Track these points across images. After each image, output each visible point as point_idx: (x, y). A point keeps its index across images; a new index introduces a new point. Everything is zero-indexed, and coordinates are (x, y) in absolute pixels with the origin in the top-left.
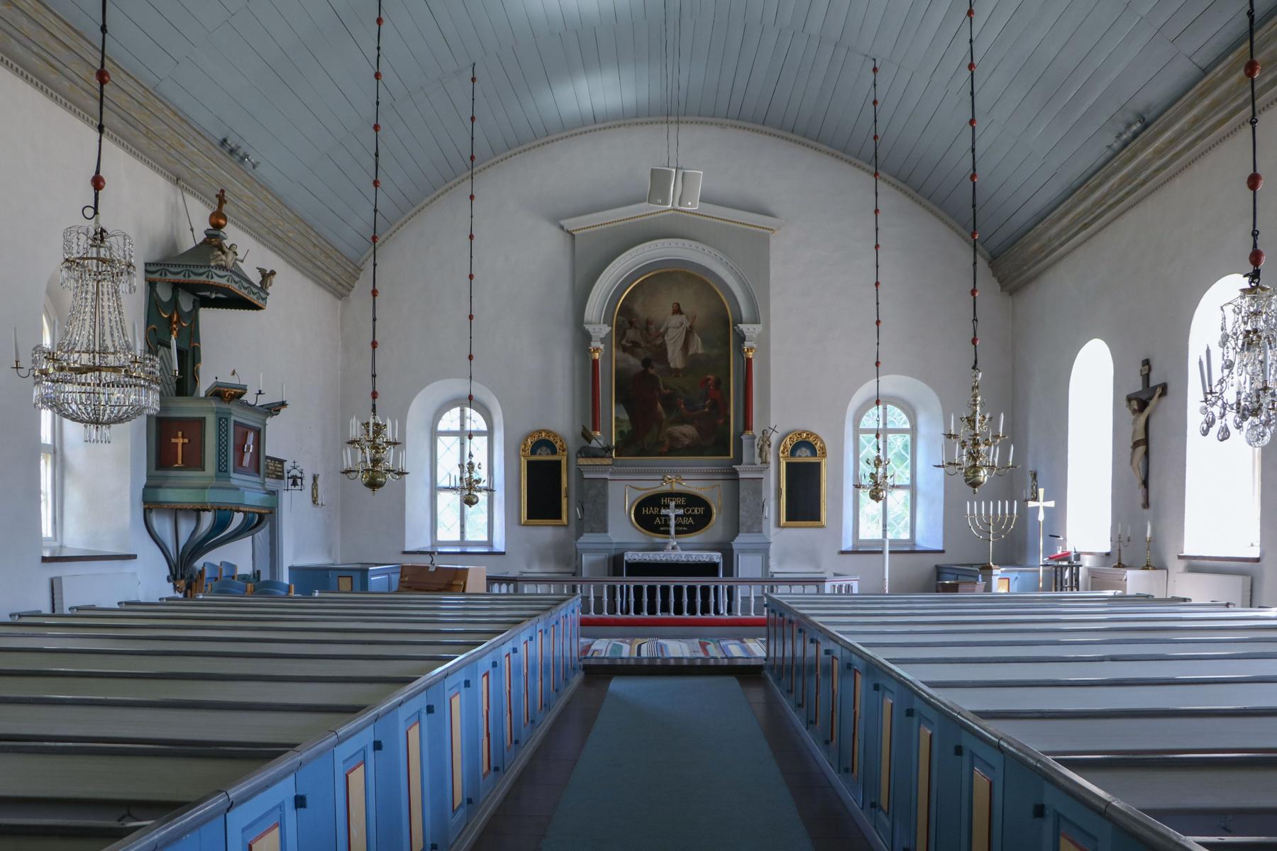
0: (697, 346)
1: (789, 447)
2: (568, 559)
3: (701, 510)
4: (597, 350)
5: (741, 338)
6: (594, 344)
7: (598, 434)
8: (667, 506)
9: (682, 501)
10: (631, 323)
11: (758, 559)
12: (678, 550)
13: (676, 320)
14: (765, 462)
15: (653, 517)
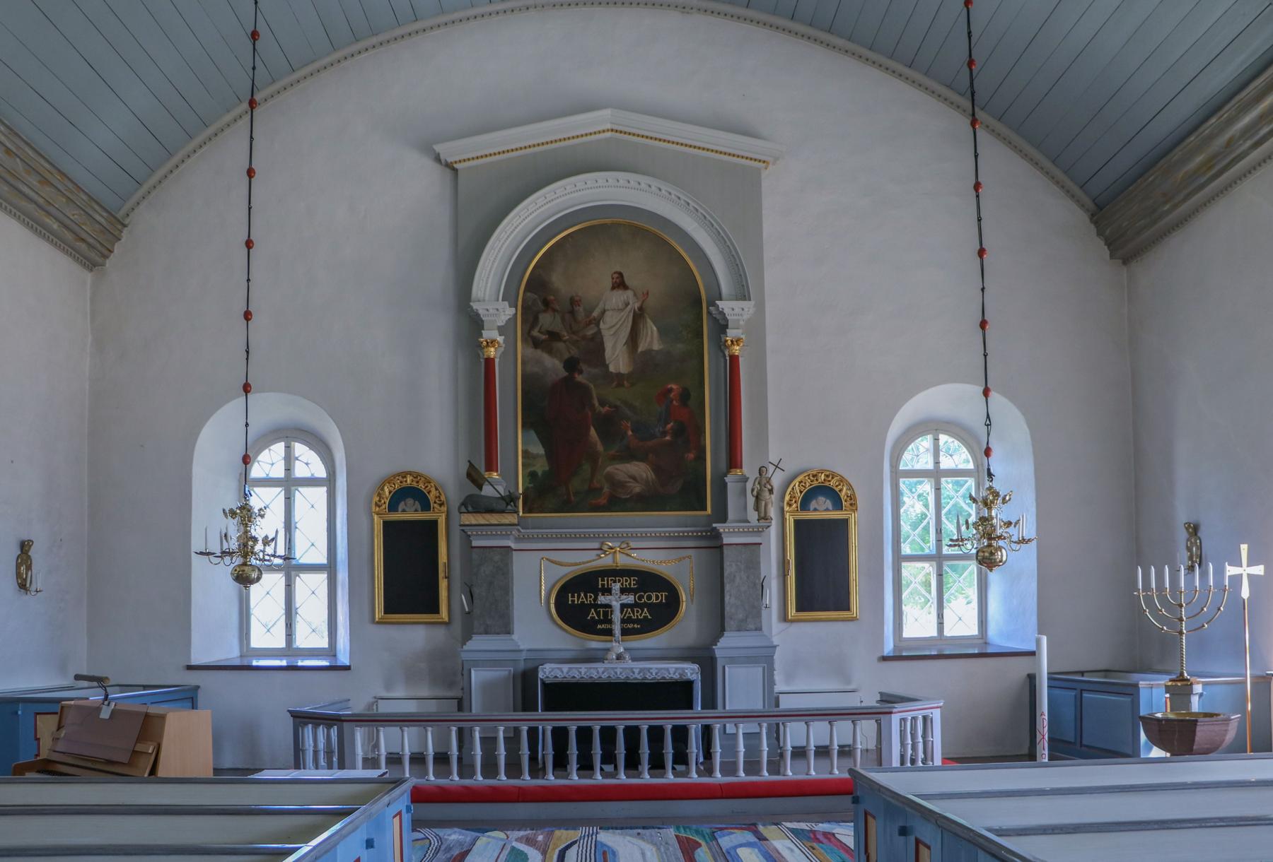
0: (651, 339)
1: (799, 496)
2: (448, 674)
3: (663, 596)
4: (492, 342)
5: (721, 326)
6: (488, 334)
7: (495, 475)
8: (608, 591)
9: (632, 582)
10: (547, 303)
11: (757, 672)
12: (625, 659)
13: (618, 298)
14: (764, 518)
15: (585, 608)
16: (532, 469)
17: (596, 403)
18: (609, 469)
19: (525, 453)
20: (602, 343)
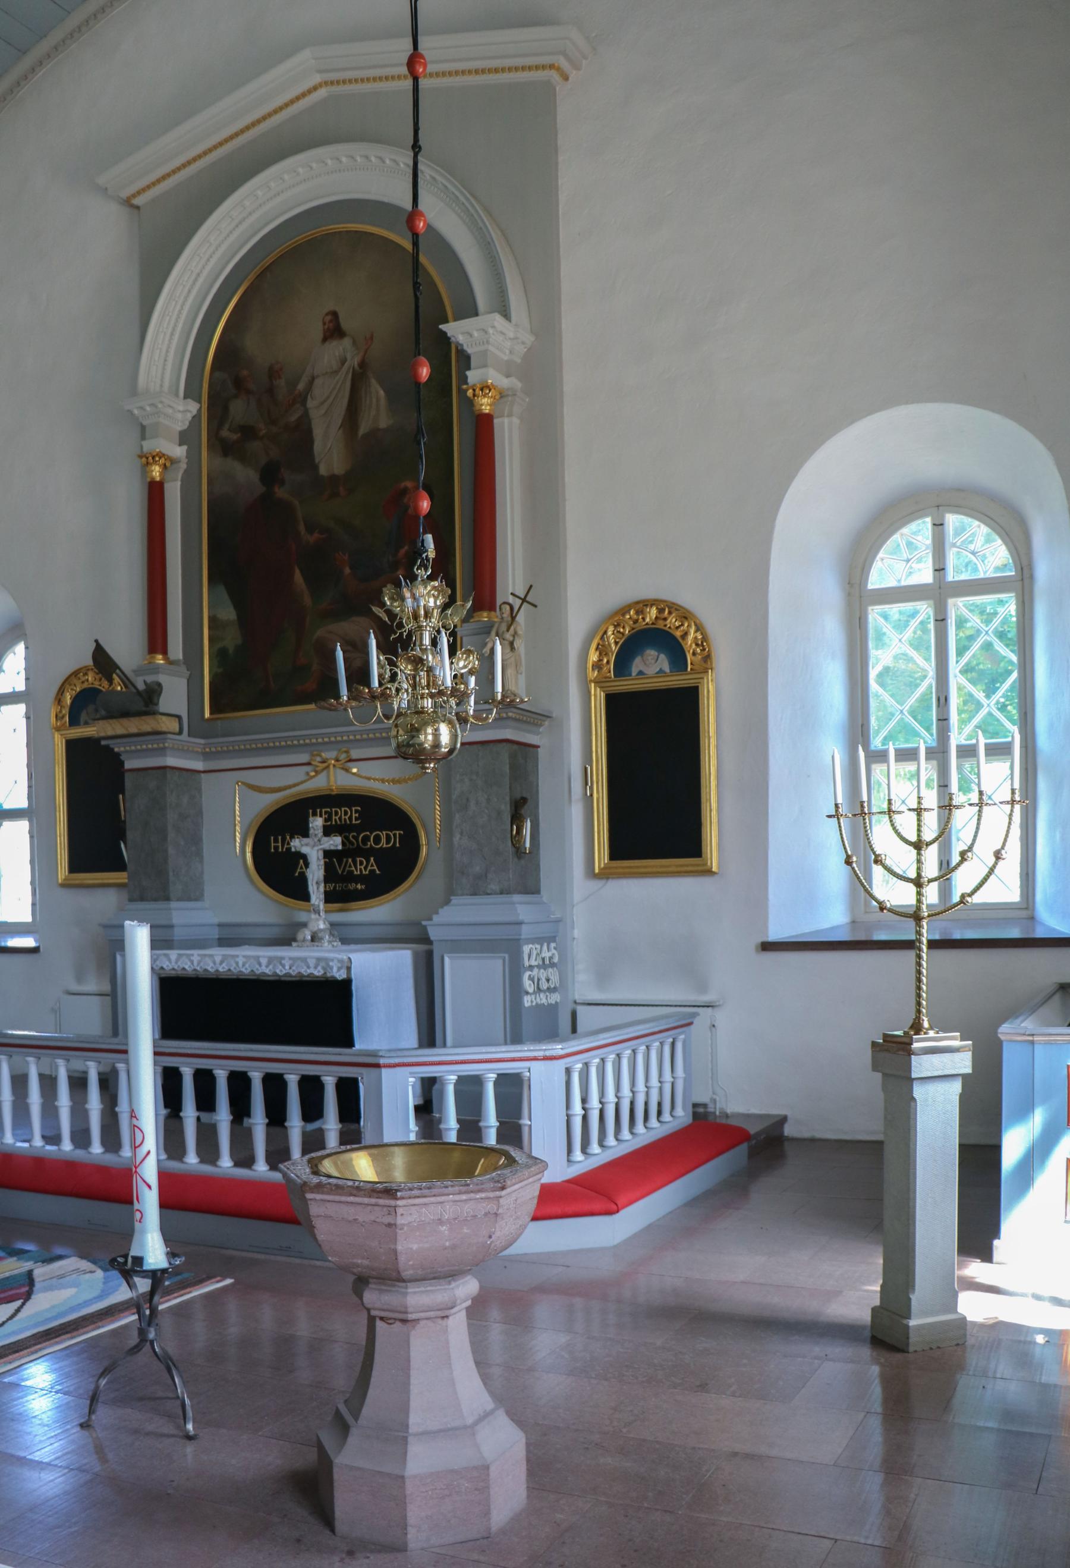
0: (378, 413)
8: (305, 833)
9: (350, 815)
10: (239, 384)
11: (495, 966)
17: (302, 528)
18: (319, 633)
19: (212, 620)
20: (309, 431)
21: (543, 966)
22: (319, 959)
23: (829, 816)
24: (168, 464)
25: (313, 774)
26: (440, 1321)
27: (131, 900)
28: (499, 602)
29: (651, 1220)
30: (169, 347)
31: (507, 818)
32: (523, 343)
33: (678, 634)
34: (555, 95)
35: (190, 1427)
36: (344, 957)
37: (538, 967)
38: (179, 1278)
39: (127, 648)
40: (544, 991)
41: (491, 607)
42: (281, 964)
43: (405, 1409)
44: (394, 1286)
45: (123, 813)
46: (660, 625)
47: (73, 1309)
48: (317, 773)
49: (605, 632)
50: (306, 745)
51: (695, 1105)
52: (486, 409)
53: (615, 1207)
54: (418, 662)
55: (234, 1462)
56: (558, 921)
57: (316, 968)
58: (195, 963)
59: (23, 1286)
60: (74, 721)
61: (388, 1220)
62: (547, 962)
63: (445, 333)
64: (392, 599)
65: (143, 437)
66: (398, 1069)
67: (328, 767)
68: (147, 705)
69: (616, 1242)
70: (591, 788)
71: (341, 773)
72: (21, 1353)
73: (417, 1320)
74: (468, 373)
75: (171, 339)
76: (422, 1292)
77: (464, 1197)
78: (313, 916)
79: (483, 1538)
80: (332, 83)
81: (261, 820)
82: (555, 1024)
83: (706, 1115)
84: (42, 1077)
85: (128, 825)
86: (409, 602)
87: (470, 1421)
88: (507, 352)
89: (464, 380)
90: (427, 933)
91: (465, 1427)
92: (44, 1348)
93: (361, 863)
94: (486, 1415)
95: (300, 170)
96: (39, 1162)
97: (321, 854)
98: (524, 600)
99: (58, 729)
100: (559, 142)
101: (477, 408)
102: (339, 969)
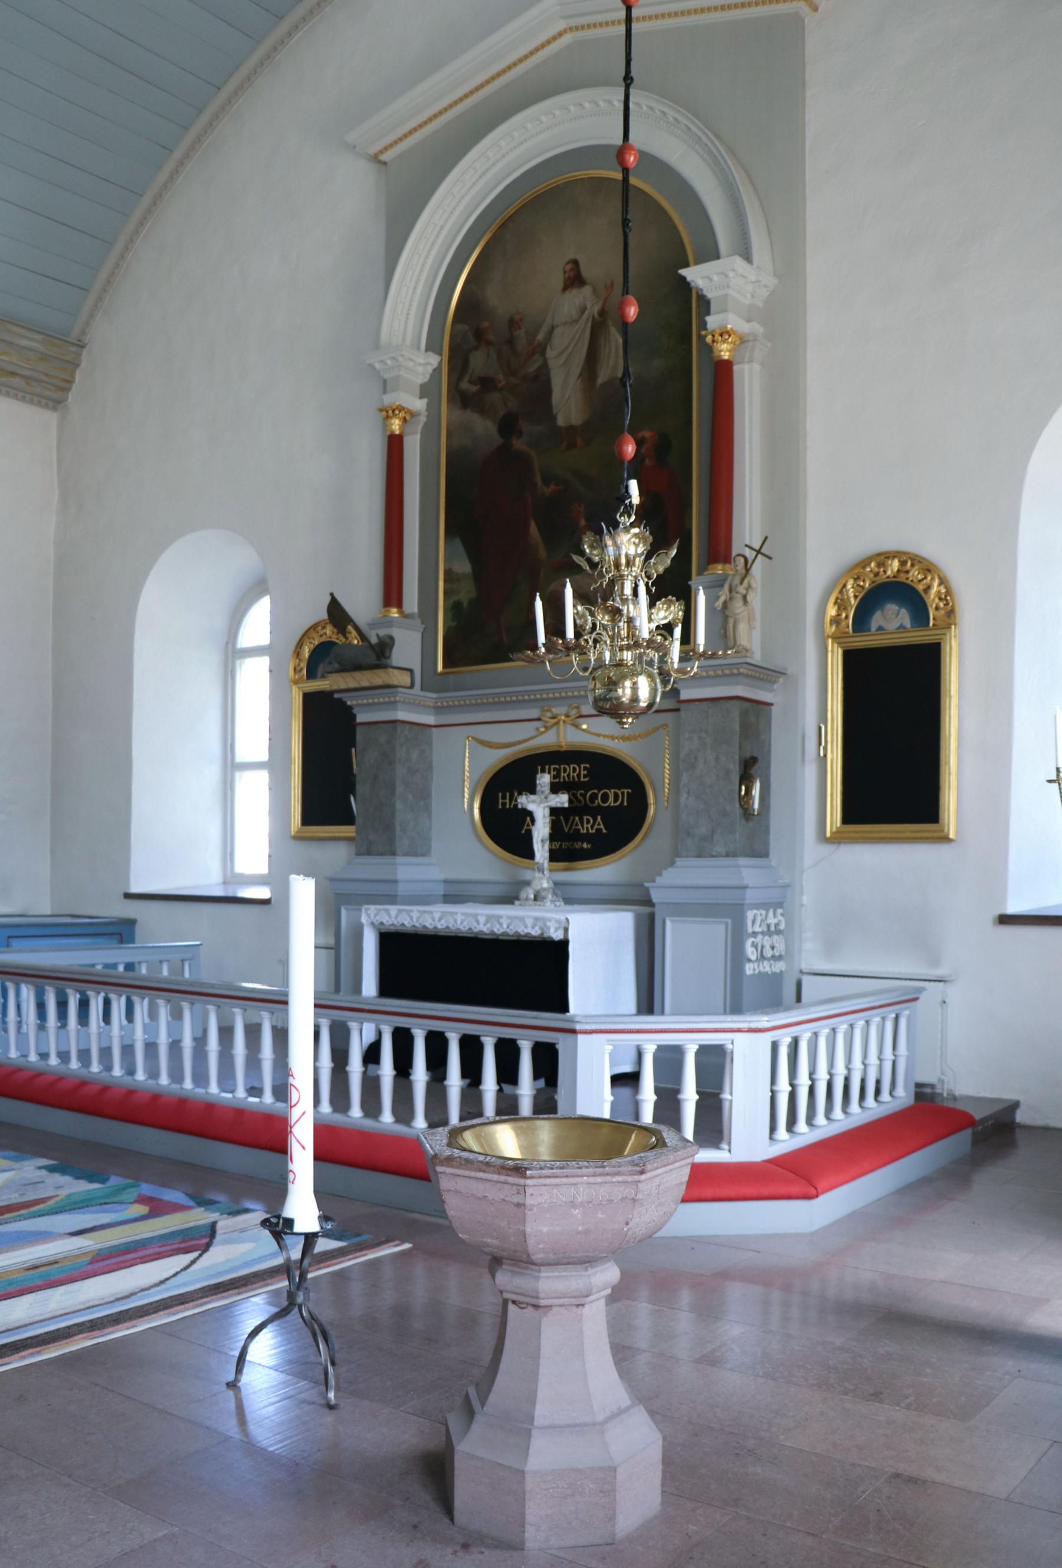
8: (532, 790)
10: (479, 335)
11: (717, 931)
16: (455, 598)
17: (539, 480)
19: (448, 573)
20: (548, 383)
21: (768, 932)
22: (536, 919)
23: (1050, 781)
24: (408, 418)
25: (542, 729)
26: (574, 1309)
27: (358, 854)
28: (734, 553)
29: (857, 1208)
30: (412, 300)
31: (736, 778)
32: (765, 286)
33: (920, 587)
34: (803, 29)
35: (331, 1395)
36: (562, 917)
37: (762, 933)
38: (358, 1239)
39: (363, 603)
40: (768, 959)
41: (727, 559)
42: (499, 923)
43: (532, 1400)
44: (527, 1268)
45: (355, 767)
46: (902, 578)
47: (246, 1264)
48: (547, 728)
49: (845, 586)
50: (537, 700)
51: (919, 1085)
52: (726, 356)
53: (814, 1192)
54: (616, 613)
55: (369, 1436)
56: (787, 886)
57: (533, 927)
58: (415, 919)
59: (205, 1237)
60: (311, 674)
61: (516, 1199)
62: (773, 928)
63: (684, 278)
64: (592, 547)
65: (385, 392)
66: (594, 1036)
67: (557, 723)
68: (378, 658)
69: (813, 1230)
70: (825, 749)
71: (570, 729)
72: (186, 1305)
73: (549, 1307)
74: (708, 318)
75: (414, 292)
76: (557, 1277)
77: (599, 1180)
78: (537, 875)
79: (607, 1544)
80: (577, 28)
81: (491, 775)
82: (776, 994)
83: (933, 1097)
84: (274, 1028)
85: (358, 778)
86: (611, 550)
87: (600, 1417)
88: (749, 295)
89: (703, 325)
90: (649, 895)
91: (594, 1424)
92: (209, 1302)
93: (588, 822)
94: (619, 1413)
95: (544, 118)
96: (239, 1114)
97: (547, 812)
98: (759, 552)
99: (296, 682)
100: (807, 77)
101: (716, 354)
102: (556, 929)
